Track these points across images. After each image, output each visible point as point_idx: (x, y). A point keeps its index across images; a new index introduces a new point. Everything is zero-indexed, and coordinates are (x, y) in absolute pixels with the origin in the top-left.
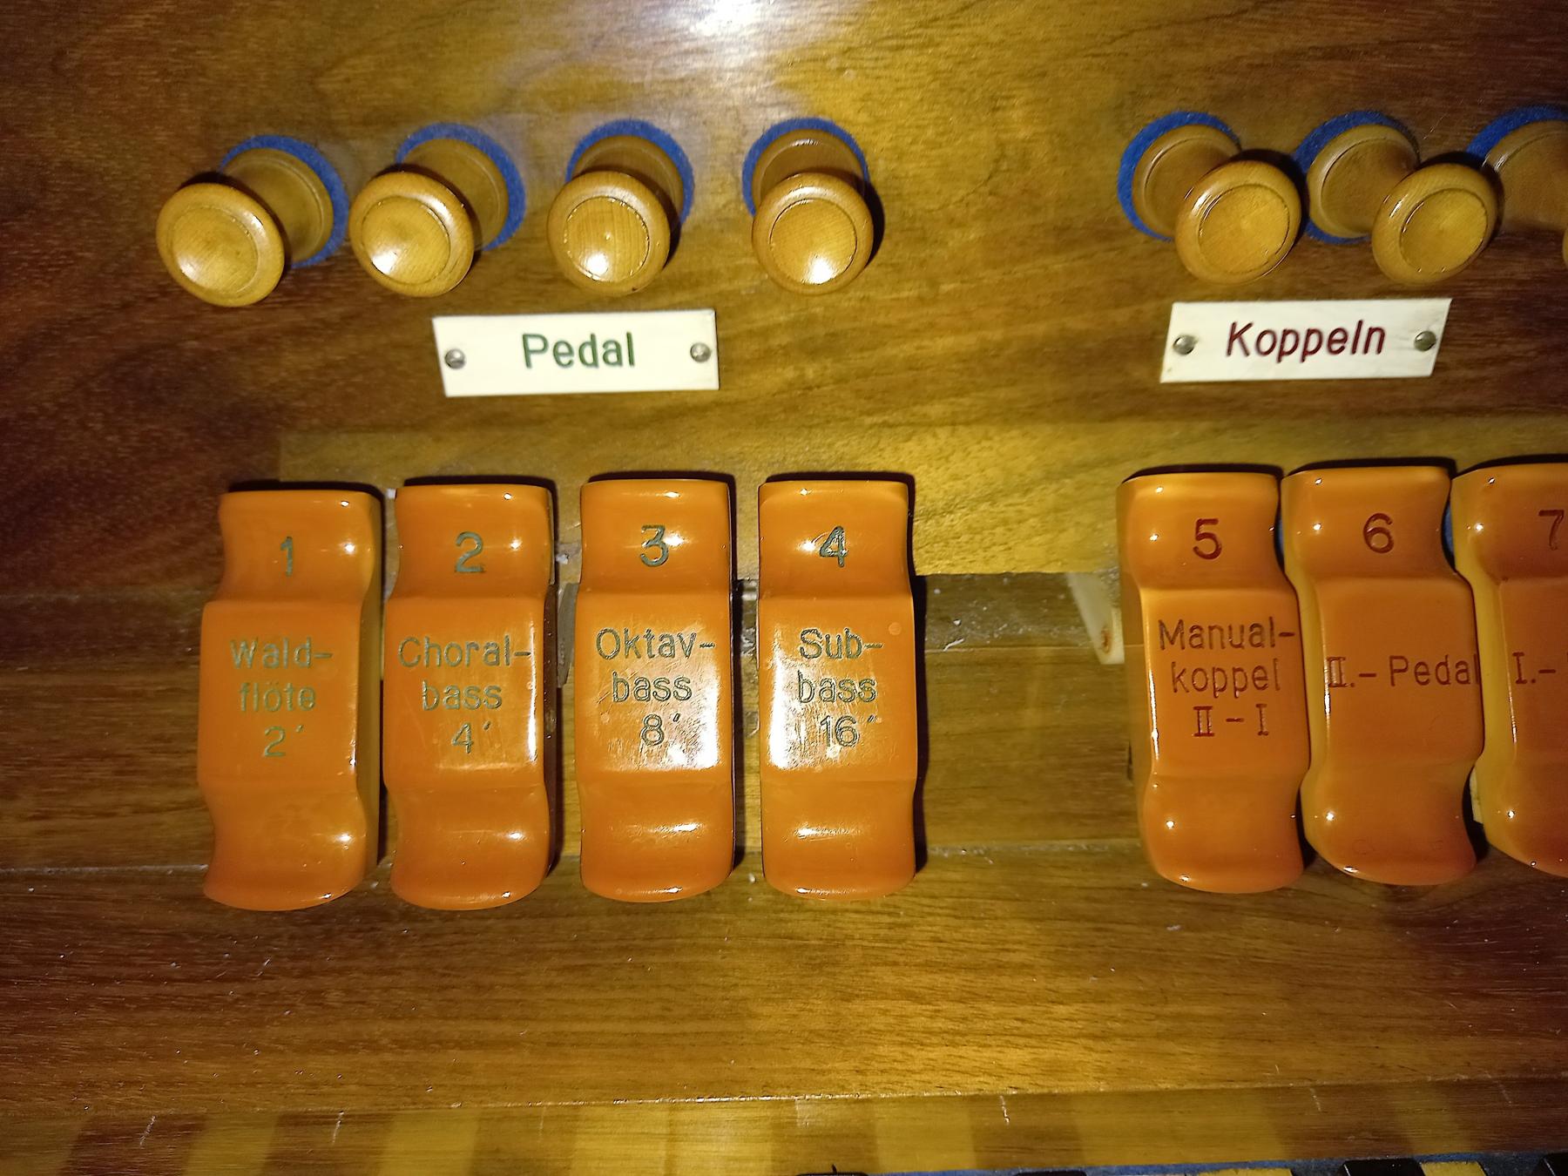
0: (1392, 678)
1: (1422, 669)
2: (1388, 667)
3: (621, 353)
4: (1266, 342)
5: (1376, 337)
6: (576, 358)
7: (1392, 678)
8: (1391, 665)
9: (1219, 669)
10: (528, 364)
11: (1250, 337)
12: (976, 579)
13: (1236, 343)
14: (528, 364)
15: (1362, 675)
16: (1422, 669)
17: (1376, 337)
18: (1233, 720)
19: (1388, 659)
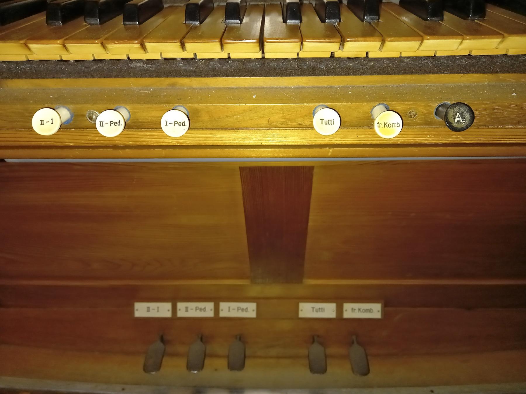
3: (322, 310)
5: (326, 123)
11: (387, 125)
17: (326, 123)
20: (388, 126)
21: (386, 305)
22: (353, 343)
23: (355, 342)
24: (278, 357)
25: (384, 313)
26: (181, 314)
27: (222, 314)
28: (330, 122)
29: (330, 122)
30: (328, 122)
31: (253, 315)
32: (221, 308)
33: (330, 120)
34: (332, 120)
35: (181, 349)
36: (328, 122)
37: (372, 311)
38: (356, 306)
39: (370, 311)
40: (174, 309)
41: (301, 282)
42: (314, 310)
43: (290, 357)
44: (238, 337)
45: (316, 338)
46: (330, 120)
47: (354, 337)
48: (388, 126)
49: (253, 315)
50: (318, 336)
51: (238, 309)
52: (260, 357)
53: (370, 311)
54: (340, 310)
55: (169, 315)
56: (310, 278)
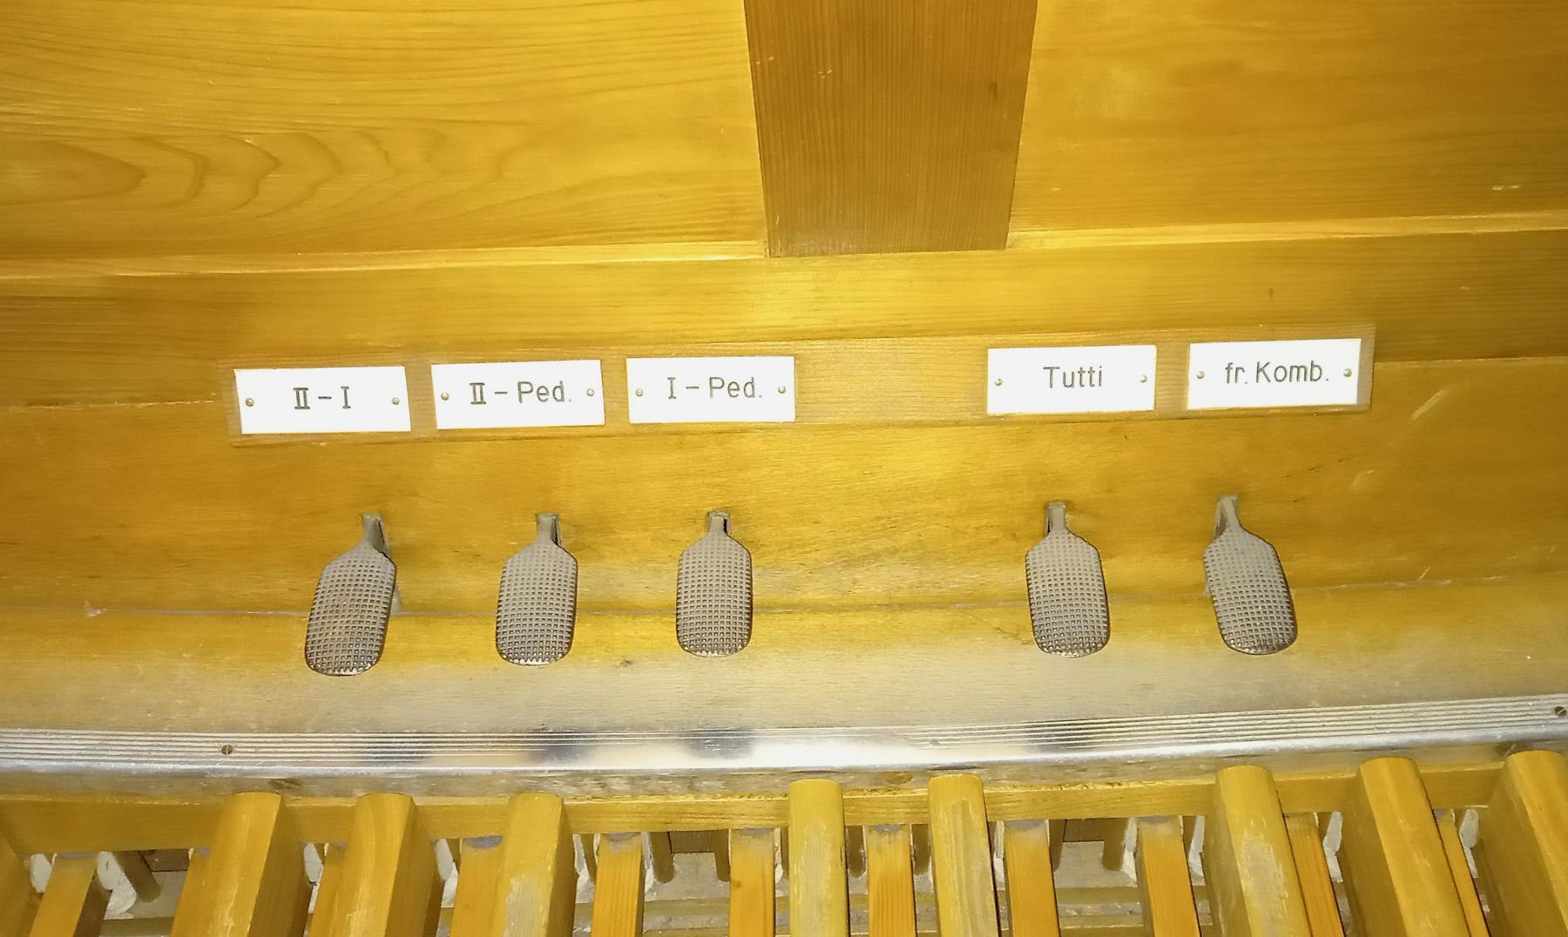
0: (1048, 368)
1: (734, 386)
2: (709, 384)
3: (1089, 377)
4: (1280, 374)
5: (1069, 382)
6: (741, 392)
7: (1048, 368)
8: (519, 389)
9: (558, 401)
10: (521, 401)
11: (1270, 371)
12: (798, 254)
13: (1261, 374)
14: (521, 401)
15: (1064, 374)
16: (734, 386)
17: (1069, 382)
18: (1051, 384)
19: (1313, 382)
20: (1271, 377)
21: (1379, 352)
22: (1221, 530)
23: (1232, 519)
24: (893, 606)
25: (1373, 384)
26: (453, 414)
27: (641, 412)
28: (1086, 377)
29: (1086, 377)
30: (1077, 376)
31: (783, 410)
32: (633, 384)
33: (1087, 369)
34: (1097, 370)
35: (469, 584)
36: (1077, 376)
37: (1316, 373)
38: (1248, 353)
39: (1310, 372)
40: (421, 396)
41: (998, 240)
42: (1058, 375)
43: (943, 604)
44: (717, 521)
45: (1058, 512)
46: (1087, 369)
47: (1227, 504)
48: (1271, 377)
49: (783, 410)
50: (1069, 506)
51: (713, 384)
52: (815, 608)
53: (1310, 372)
54: (1173, 372)
55: (398, 421)
56: (1040, 220)
